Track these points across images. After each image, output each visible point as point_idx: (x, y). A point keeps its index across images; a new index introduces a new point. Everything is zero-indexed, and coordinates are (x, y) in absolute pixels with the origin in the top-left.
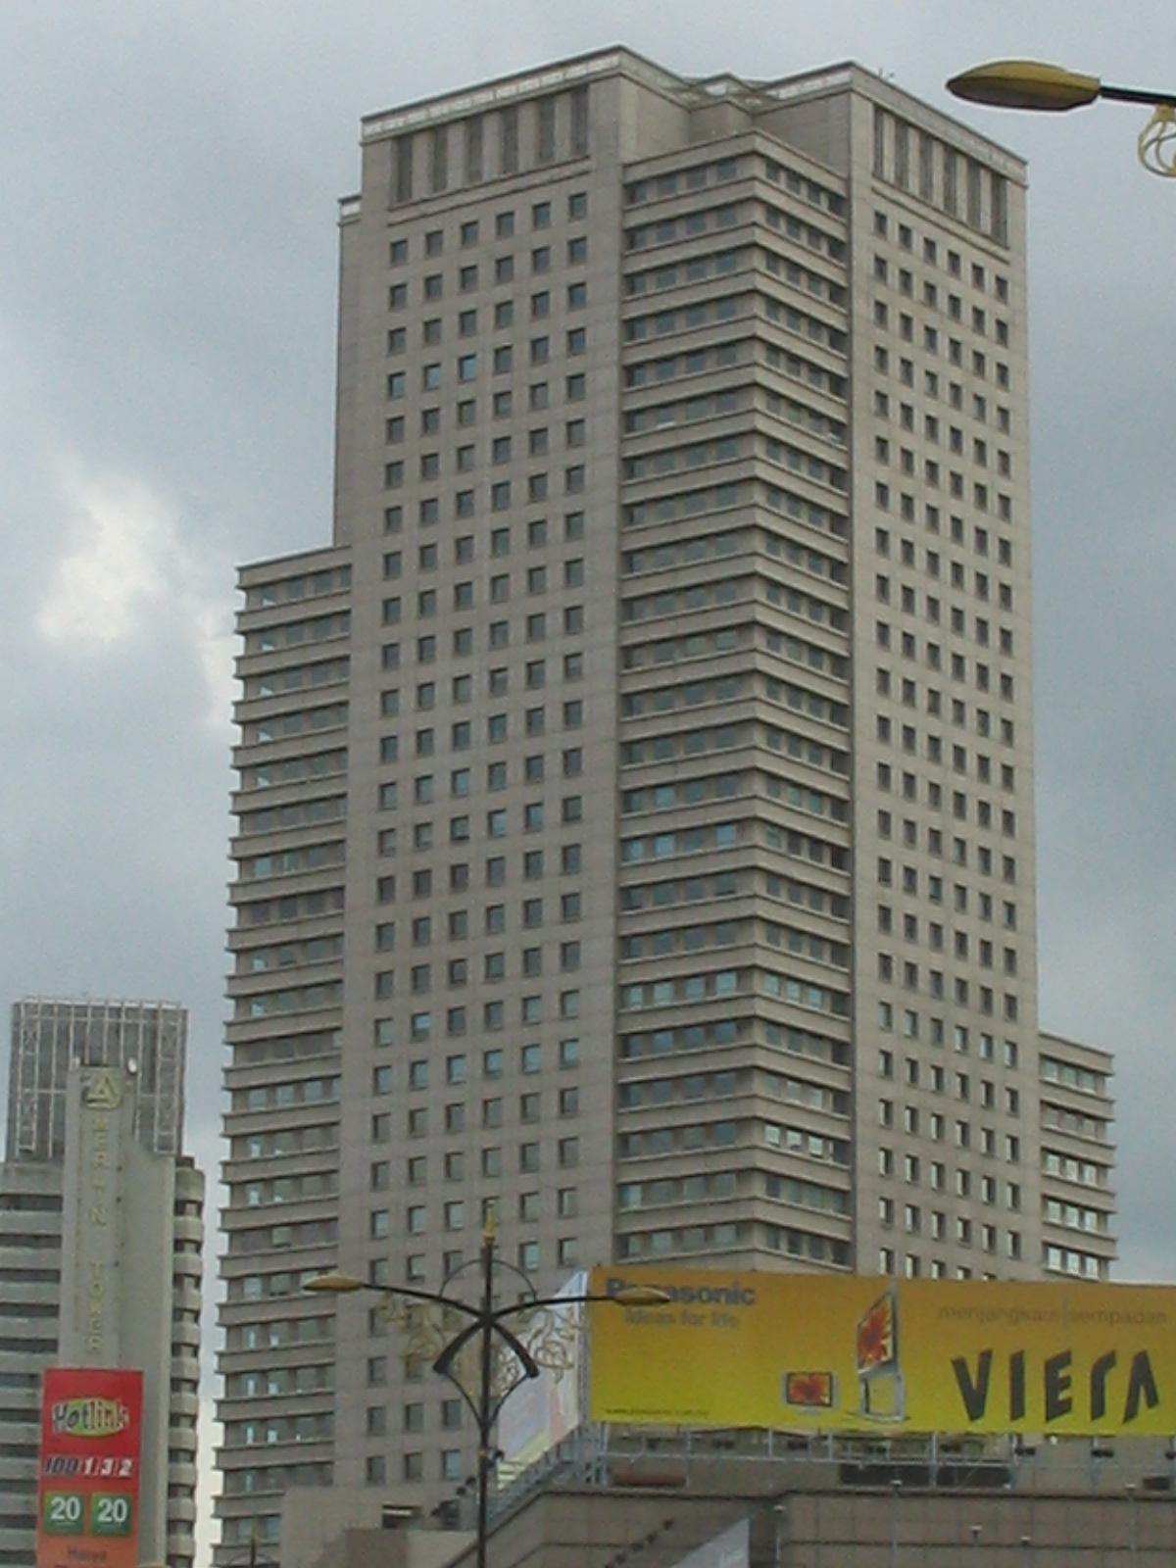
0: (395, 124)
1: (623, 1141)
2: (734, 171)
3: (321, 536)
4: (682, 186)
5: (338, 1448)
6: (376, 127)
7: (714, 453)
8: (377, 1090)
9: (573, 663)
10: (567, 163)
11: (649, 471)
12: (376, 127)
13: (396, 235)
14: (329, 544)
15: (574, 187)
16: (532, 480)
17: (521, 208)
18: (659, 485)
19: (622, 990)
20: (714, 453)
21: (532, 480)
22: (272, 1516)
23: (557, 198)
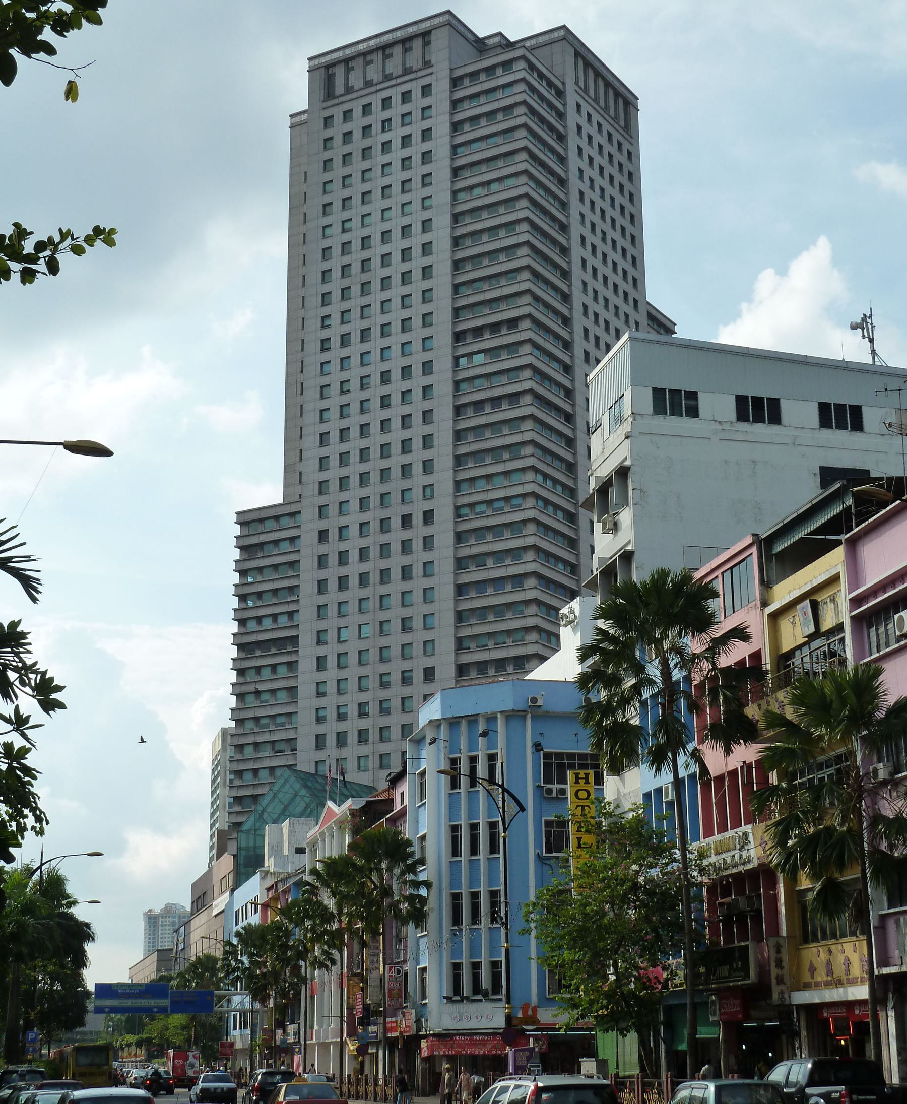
0: (323, 60)
1: (457, 484)
2: (520, 349)
3: (277, 498)
4: (483, 122)
5: (300, 755)
6: (317, 62)
7: (504, 255)
8: (322, 420)
9: (427, 295)
10: (420, 70)
11: (466, 173)
12: (317, 62)
13: (327, 113)
14: (281, 501)
15: (426, 81)
16: (403, 417)
17: (396, 95)
18: (471, 179)
19: (456, 359)
20: (504, 255)
21: (403, 417)
22: (260, 795)
23: (415, 88)
